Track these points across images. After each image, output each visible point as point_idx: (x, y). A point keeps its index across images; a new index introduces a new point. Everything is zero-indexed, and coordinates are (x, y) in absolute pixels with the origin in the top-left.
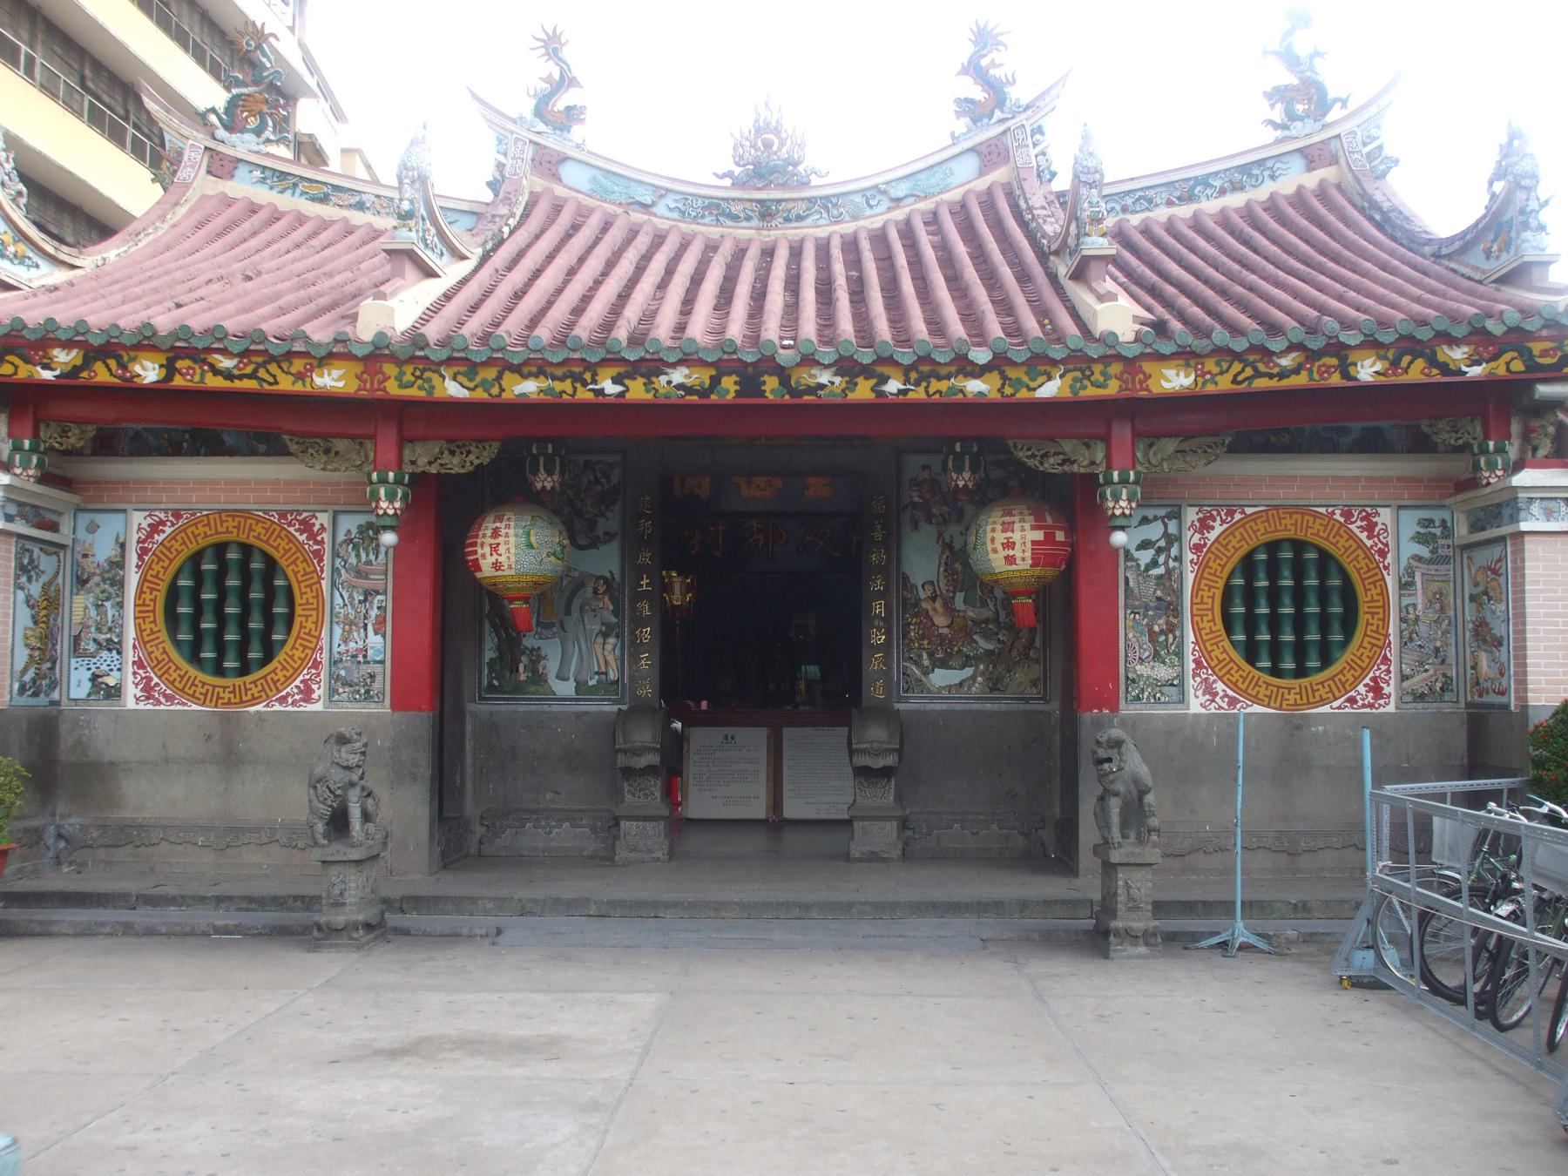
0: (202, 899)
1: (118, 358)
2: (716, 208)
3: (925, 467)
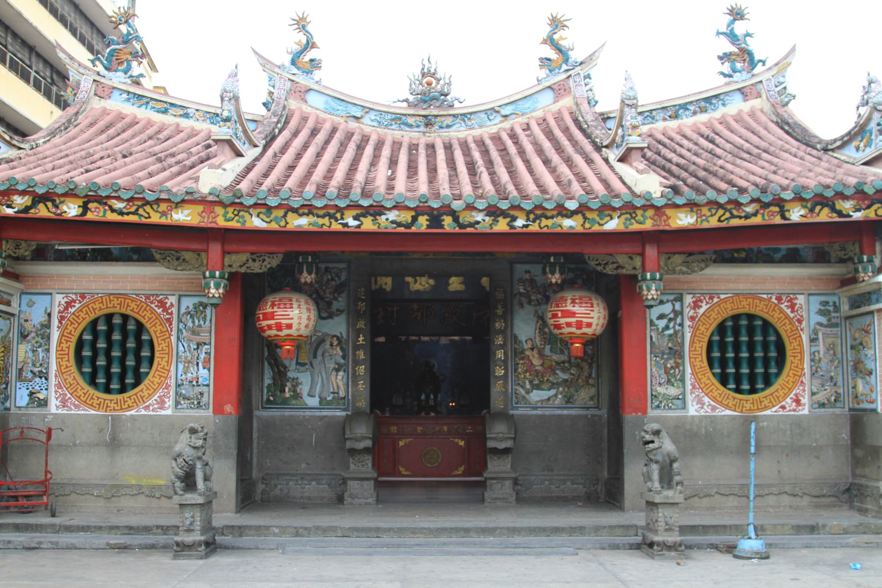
0: (100, 528)
1: (53, 201)
2: (399, 119)
3: (527, 272)
